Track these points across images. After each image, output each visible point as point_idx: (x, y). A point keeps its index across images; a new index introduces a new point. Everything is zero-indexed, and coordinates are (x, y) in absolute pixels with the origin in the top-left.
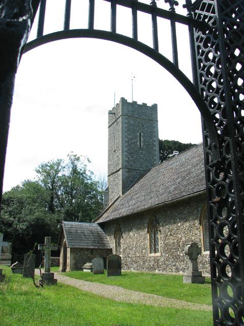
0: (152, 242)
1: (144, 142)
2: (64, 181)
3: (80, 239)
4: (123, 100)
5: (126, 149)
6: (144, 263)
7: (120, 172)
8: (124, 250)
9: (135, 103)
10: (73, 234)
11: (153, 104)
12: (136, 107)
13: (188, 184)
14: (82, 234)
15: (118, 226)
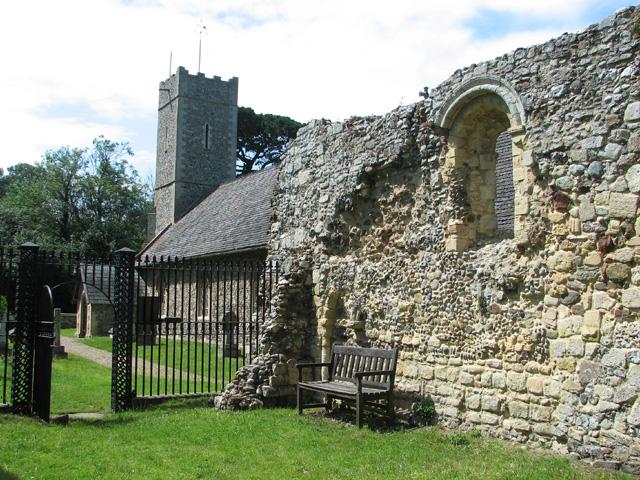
1: (213, 140)
2: (88, 186)
4: (182, 71)
7: (173, 187)
9: (201, 75)
12: (203, 82)
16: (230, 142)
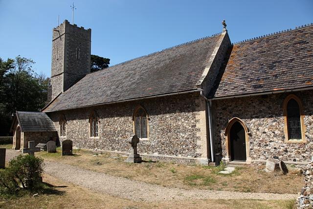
5: (67, 59)
15: (64, 116)
16: (88, 57)
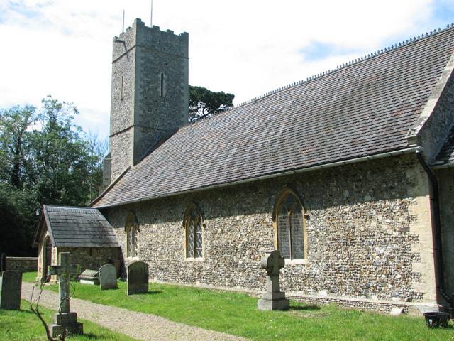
0: (190, 241)
1: (168, 88)
2: (36, 141)
3: (73, 232)
4: (139, 23)
6: (176, 271)
8: (142, 250)
9: (156, 28)
10: (61, 224)
11: (183, 32)
13: (252, 159)
14: (76, 225)
16: (182, 91)
